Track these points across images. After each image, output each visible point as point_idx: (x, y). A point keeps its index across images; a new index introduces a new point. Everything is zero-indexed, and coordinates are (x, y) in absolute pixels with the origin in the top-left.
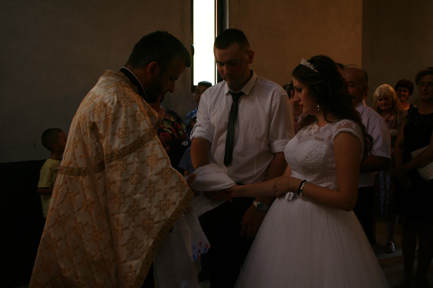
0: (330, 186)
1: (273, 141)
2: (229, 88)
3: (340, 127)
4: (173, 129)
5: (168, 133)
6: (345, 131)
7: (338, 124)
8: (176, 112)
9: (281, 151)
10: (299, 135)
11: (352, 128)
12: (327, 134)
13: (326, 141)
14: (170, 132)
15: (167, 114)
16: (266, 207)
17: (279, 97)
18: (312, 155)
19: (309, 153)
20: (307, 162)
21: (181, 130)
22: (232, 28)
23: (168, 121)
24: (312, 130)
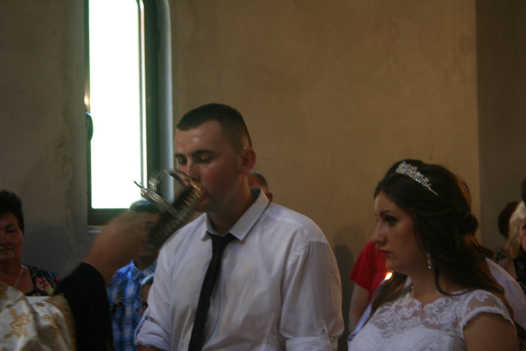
2: (208, 228)
12: (447, 317)
15: (38, 278)
17: (304, 246)
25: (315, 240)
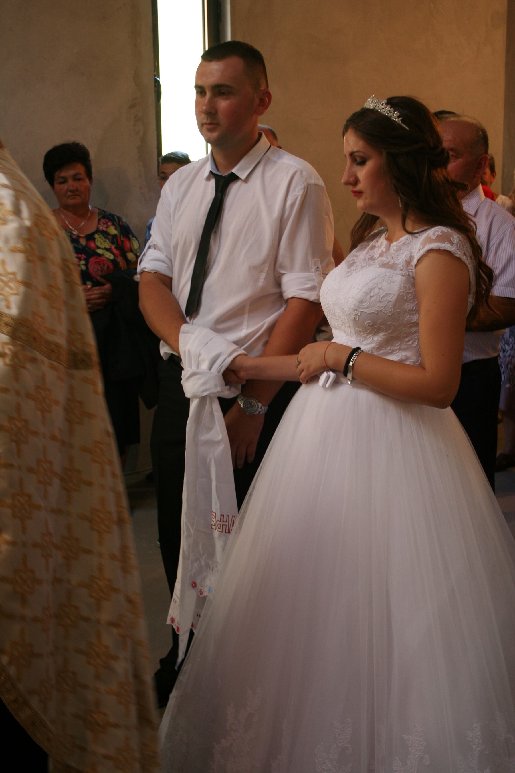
0: (407, 358)
1: (284, 274)
2: (211, 167)
3: (429, 240)
4: (115, 251)
5: (106, 258)
6: (437, 248)
7: (424, 236)
8: (118, 215)
9: (297, 294)
10: (351, 259)
11: (452, 243)
13: (401, 270)
14: (110, 256)
15: (102, 220)
16: (261, 408)
17: (303, 186)
18: (371, 297)
19: (367, 294)
20: (362, 310)
21: (131, 250)
22: (239, 39)
23: (105, 234)
24: (376, 250)
25: (313, 182)
